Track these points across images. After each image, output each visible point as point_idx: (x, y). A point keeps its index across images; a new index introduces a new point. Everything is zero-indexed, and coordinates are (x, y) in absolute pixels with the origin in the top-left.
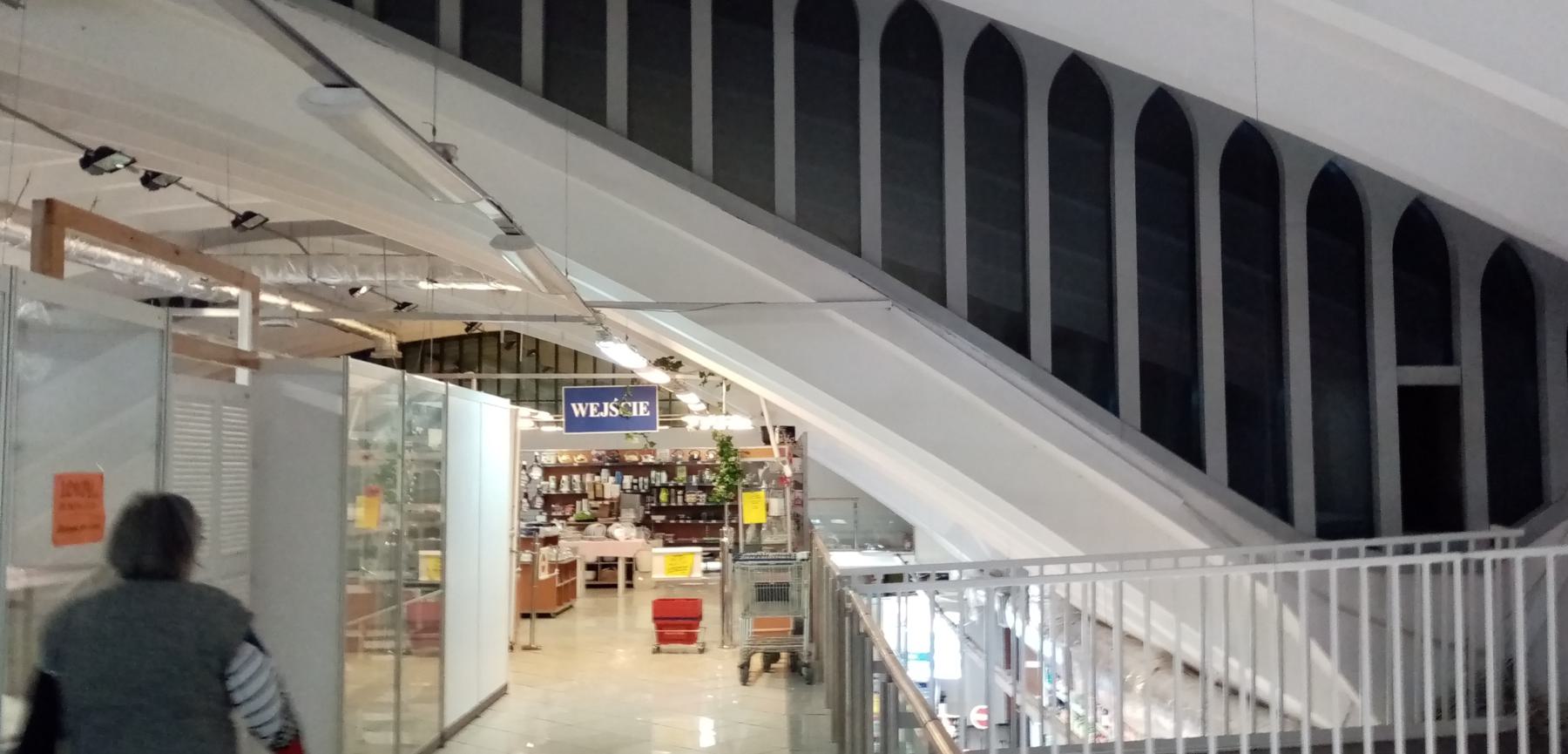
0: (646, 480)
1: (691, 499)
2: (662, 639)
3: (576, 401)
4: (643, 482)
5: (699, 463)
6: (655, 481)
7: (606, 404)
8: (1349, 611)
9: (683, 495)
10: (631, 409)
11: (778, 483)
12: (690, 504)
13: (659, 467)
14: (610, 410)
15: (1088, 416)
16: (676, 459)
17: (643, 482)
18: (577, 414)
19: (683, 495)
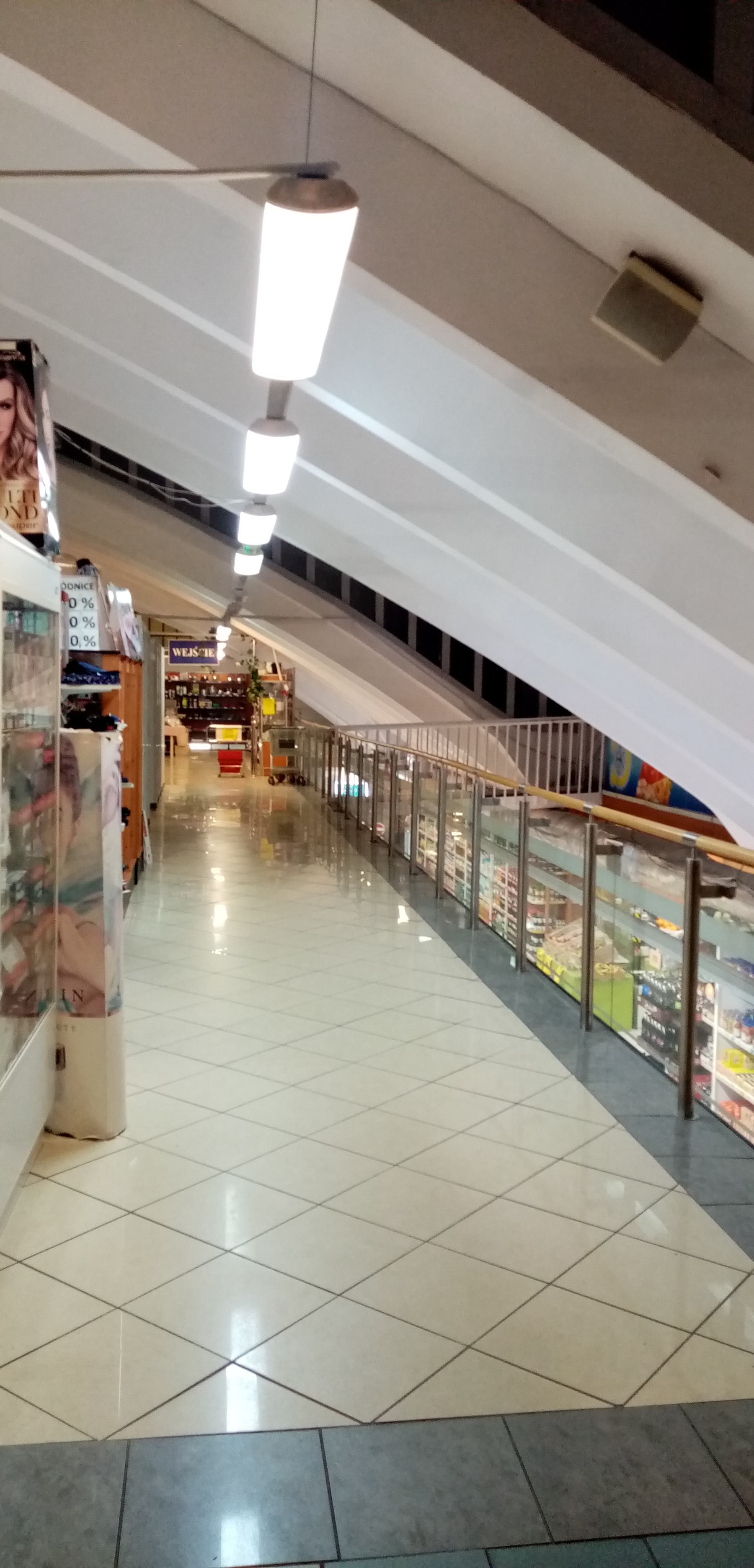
0: (174, 692)
1: (202, 704)
2: (223, 770)
3: (176, 647)
4: (172, 693)
5: (208, 682)
6: (179, 692)
7: (191, 650)
8: (523, 745)
9: (197, 702)
10: (204, 653)
11: (281, 694)
12: (202, 708)
13: (181, 683)
14: (193, 653)
15: (428, 667)
16: (192, 679)
17: (172, 693)
18: (176, 654)
19: (197, 702)
